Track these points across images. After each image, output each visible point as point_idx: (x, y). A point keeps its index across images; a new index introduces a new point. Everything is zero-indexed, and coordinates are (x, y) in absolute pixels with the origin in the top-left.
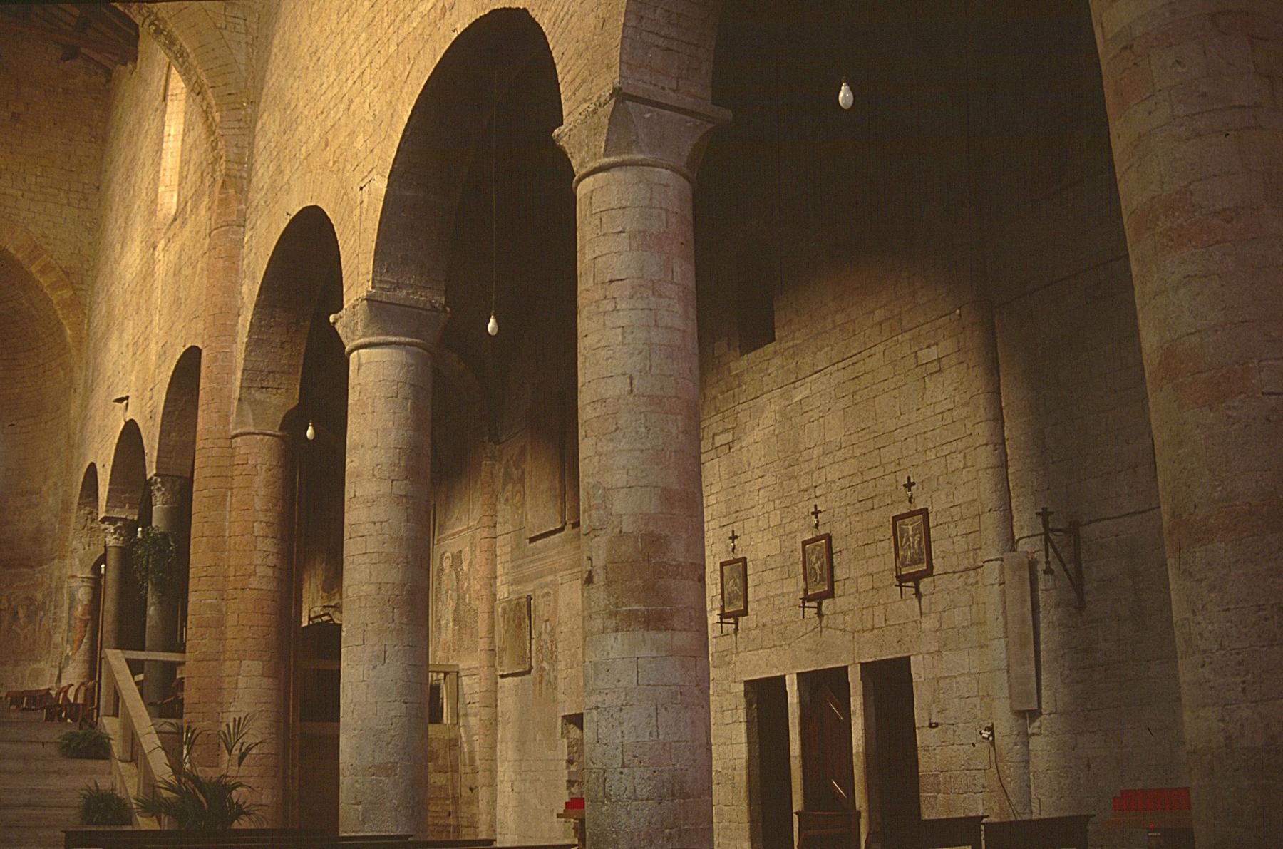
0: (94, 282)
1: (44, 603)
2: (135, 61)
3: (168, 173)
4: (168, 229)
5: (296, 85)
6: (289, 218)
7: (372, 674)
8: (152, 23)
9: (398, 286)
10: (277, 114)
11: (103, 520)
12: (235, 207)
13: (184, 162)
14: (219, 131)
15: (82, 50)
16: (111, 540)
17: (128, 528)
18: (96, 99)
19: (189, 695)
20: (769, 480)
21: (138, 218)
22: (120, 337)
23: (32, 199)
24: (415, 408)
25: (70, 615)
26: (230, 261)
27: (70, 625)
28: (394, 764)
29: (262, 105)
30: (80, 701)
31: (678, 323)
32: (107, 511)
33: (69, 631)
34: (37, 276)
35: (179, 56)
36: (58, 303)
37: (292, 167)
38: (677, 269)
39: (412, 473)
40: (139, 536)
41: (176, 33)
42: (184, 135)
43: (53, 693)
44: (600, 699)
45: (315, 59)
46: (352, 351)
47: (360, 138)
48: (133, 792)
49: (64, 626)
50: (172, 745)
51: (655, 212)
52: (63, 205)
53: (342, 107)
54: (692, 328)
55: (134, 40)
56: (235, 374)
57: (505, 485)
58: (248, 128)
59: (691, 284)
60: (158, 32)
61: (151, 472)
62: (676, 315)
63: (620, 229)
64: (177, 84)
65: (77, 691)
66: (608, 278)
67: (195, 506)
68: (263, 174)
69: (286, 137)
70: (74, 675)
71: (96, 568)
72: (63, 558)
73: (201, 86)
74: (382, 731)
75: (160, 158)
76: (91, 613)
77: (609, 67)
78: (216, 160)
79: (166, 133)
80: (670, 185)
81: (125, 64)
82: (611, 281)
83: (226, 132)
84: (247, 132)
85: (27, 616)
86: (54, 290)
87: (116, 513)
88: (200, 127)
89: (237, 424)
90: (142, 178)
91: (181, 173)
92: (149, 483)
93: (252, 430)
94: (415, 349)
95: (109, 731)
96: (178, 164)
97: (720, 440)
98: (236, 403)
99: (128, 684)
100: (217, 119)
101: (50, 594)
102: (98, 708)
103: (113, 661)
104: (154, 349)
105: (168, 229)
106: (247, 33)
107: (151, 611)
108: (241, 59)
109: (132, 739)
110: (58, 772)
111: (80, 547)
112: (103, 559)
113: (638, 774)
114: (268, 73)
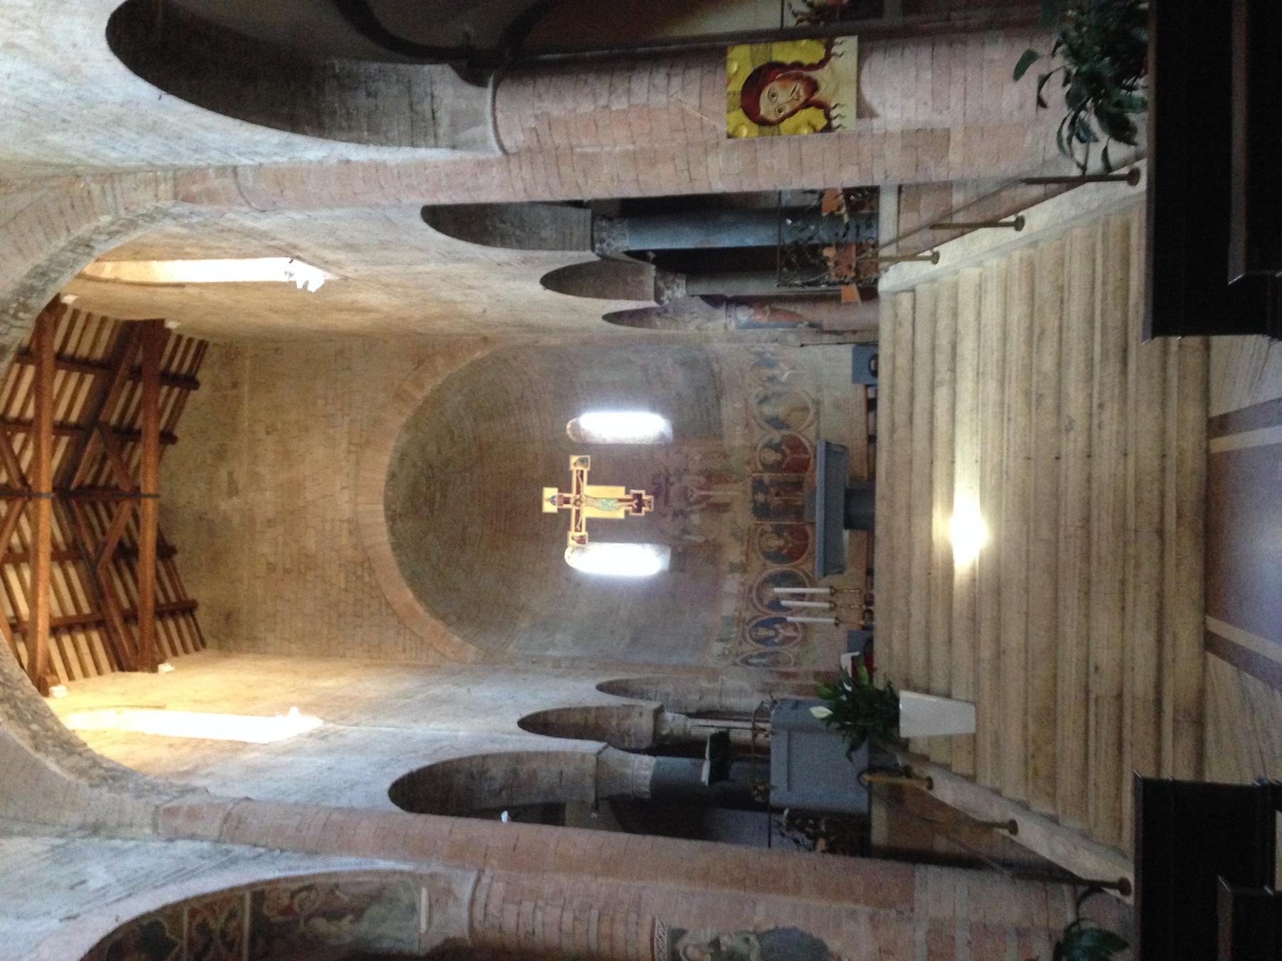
8: (15, 316)
12: (215, 183)
23: (350, 405)
26: (282, 187)
32: (649, 299)
61: (589, 256)
76: (762, 306)
93: (490, 127)
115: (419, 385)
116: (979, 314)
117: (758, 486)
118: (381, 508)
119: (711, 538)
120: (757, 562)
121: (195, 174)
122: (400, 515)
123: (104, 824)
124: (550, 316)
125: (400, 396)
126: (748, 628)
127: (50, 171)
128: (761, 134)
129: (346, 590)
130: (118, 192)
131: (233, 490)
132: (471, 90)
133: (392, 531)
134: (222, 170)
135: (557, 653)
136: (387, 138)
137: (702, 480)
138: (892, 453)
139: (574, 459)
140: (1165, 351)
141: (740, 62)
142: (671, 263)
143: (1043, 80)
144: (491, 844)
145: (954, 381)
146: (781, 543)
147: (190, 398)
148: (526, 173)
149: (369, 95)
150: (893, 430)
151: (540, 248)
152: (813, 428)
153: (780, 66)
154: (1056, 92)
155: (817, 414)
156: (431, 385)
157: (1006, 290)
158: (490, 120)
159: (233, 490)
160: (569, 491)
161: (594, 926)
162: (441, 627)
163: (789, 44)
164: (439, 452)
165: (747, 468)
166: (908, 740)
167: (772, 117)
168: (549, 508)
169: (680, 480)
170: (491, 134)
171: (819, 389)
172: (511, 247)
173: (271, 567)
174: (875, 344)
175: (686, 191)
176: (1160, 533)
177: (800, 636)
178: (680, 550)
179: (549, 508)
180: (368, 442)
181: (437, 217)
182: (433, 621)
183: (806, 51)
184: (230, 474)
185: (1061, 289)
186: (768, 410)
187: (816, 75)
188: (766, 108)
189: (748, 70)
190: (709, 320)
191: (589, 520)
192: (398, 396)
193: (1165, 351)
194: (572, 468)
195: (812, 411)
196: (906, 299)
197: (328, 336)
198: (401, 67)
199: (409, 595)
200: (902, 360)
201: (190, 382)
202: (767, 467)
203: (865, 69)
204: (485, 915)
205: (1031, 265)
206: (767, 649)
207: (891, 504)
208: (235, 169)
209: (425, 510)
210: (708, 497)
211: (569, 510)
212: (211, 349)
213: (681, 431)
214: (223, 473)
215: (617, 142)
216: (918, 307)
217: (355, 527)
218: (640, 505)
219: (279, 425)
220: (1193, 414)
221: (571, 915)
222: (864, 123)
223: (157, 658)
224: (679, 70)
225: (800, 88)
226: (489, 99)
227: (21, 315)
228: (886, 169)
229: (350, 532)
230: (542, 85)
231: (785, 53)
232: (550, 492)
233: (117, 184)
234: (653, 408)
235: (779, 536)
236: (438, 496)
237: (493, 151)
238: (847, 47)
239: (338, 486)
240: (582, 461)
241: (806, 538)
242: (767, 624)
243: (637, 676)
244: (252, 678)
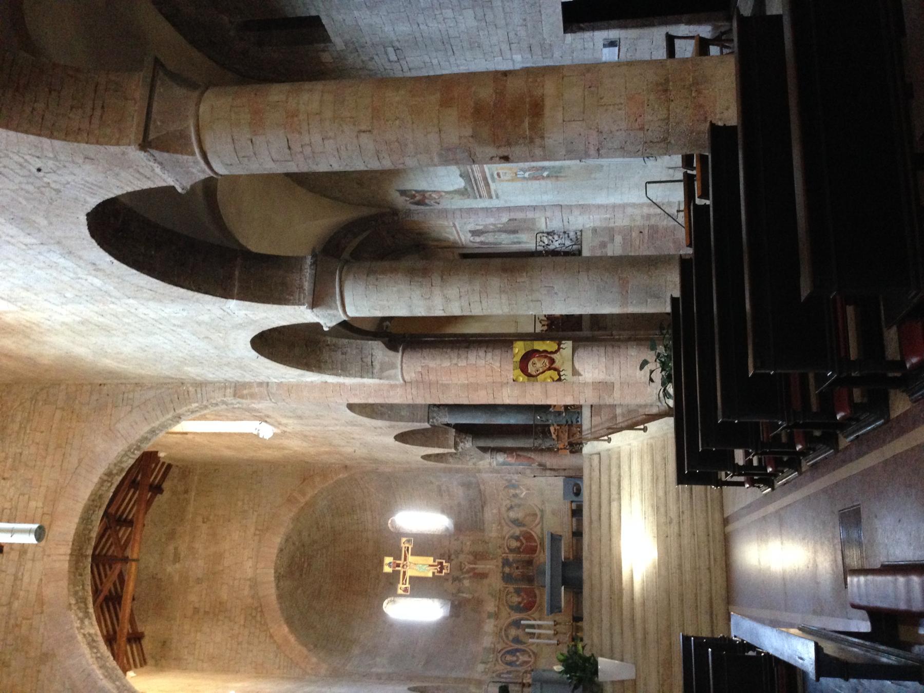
0: (307, 463)
7: (560, 294)
9: (301, 287)
11: (456, 448)
12: (256, 390)
14: (205, 403)
20: (421, 19)
24: (384, 272)
28: (620, 279)
31: (316, 96)
34: (308, 498)
38: (276, 98)
39: (425, 273)
44: (592, 148)
46: (347, 316)
47: (200, 318)
51: (233, 116)
53: (179, 330)
54: (319, 86)
57: (426, 205)
59: (286, 87)
61: (426, 425)
62: (311, 98)
63: (249, 142)
66: (288, 151)
68: (232, 374)
73: (175, 417)
74: (598, 287)
77: (123, 154)
80: (214, 104)
82: (289, 148)
87: (452, 443)
89: (397, 380)
92: (433, 426)
94: (343, 274)
97: (393, 57)
113: (650, 118)
115: (304, 495)
116: (630, 467)
117: (506, 562)
118: (273, 571)
119: (476, 595)
120: (505, 611)
121: (245, 385)
122: (283, 576)
124: (391, 455)
125: (291, 500)
126: (500, 655)
127: (170, 381)
128: (529, 380)
130: (204, 393)
131: (177, 558)
132: (391, 353)
133: (278, 587)
134: (260, 384)
135: (380, 670)
137: (472, 558)
138: (591, 535)
139: (404, 540)
140: (706, 489)
141: (520, 348)
142: (463, 430)
143: (652, 372)
145: (620, 499)
146: (520, 599)
147: (157, 499)
148: (414, 391)
149: (342, 354)
150: (591, 522)
151: (401, 421)
152: (539, 526)
153: (537, 351)
154: (658, 376)
155: (542, 517)
156: (310, 493)
157: (641, 458)
158: (399, 367)
159: (177, 558)
160: (400, 559)
162: (305, 651)
163: (541, 342)
165: (499, 550)
166: (602, 682)
167: (534, 373)
168: (387, 569)
169: (457, 557)
171: (543, 502)
172: (386, 420)
173: (196, 610)
174: (581, 478)
175: (492, 403)
176: (709, 569)
177: (533, 660)
178: (456, 603)
179: (387, 569)
180: (268, 529)
181: (351, 407)
182: (300, 647)
183: (549, 346)
184: (176, 549)
185: (664, 458)
186: (512, 515)
187: (554, 356)
188: (531, 369)
189: (523, 352)
190: (481, 460)
191: (411, 577)
192: (289, 500)
193: (706, 489)
194: (402, 545)
195: (539, 517)
196: (596, 458)
197: (251, 462)
198: (359, 341)
199: (286, 629)
200: (595, 487)
201: (157, 489)
202: (511, 551)
203: (576, 355)
205: (652, 446)
206: (513, 669)
207: (591, 561)
208: (268, 383)
209: (297, 574)
210: (474, 569)
211: (399, 571)
212: (173, 469)
213: (459, 527)
214: (171, 548)
215: (460, 379)
216: (568, 258)
217: (254, 584)
218: (442, 568)
219: (211, 518)
220: (717, 516)
222: (575, 378)
223: (127, 667)
224: (490, 350)
225: (547, 361)
226: (400, 357)
228: (586, 398)
229: (251, 587)
230: (426, 352)
231: (540, 346)
232: (388, 560)
233: (204, 388)
234: (443, 511)
235: (519, 595)
236: (306, 565)
238: (568, 345)
239: (247, 556)
240: (408, 541)
241: (535, 596)
242: (513, 652)
243: (430, 685)
244: (190, 681)
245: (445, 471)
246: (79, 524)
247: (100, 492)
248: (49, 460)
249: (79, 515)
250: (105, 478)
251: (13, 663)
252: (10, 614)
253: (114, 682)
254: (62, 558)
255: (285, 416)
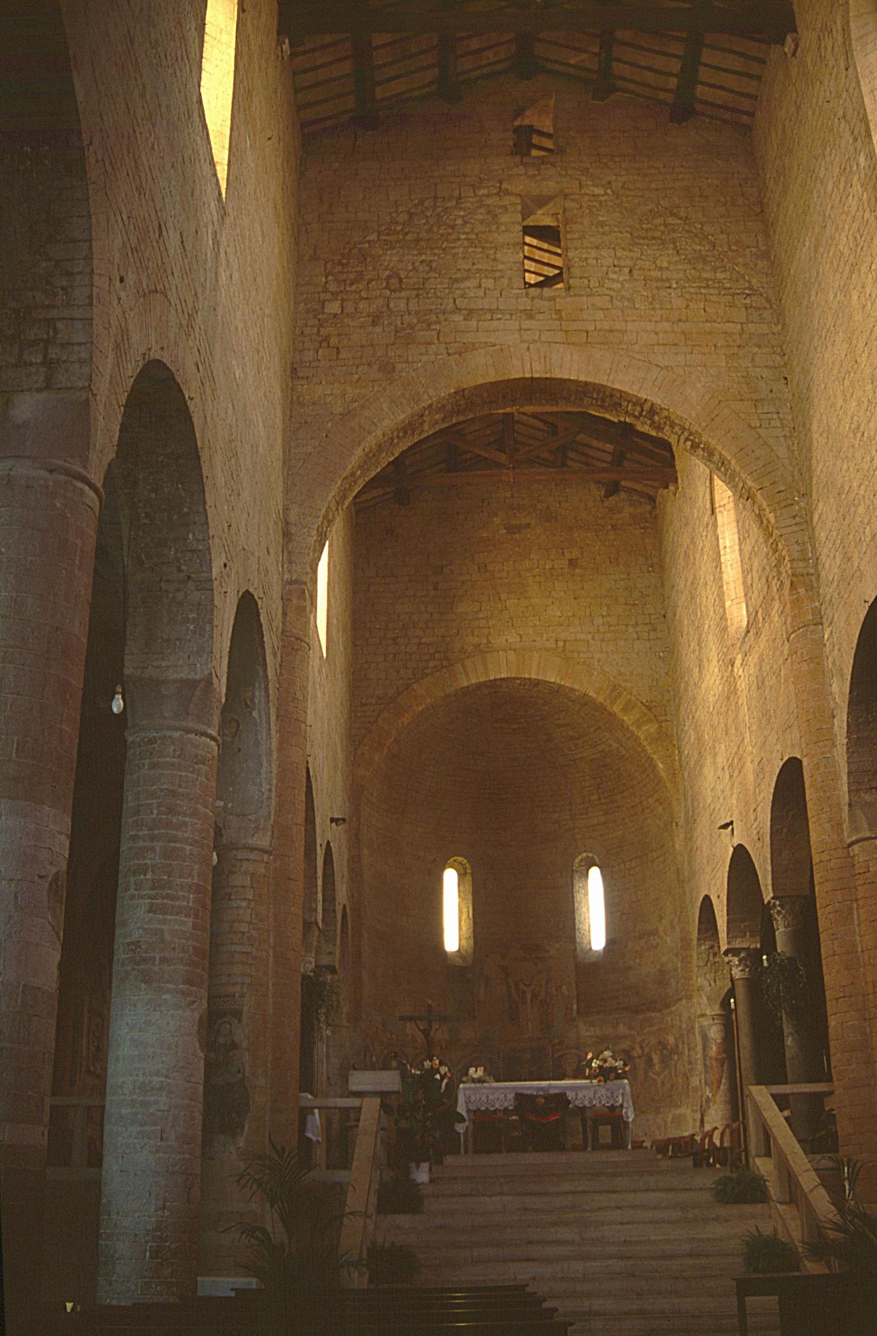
0: (678, 709)
1: (677, 1045)
2: (676, 481)
3: (732, 586)
4: (743, 642)
5: (845, 467)
6: (867, 606)
8: (687, 439)
10: (832, 500)
11: (726, 953)
13: (746, 571)
15: (623, 483)
16: (737, 973)
17: (752, 958)
18: (645, 528)
19: (843, 1127)
21: (710, 636)
22: (714, 763)
23: (602, 640)
25: (705, 1056)
27: (705, 1065)
29: (814, 495)
30: (726, 1145)
32: (729, 943)
33: (706, 1072)
34: (620, 715)
35: (721, 466)
36: (646, 739)
37: (859, 553)
40: (765, 964)
41: (713, 443)
42: (740, 544)
43: (698, 1138)
45: (859, 435)
48: (796, 1235)
49: (700, 1067)
50: (831, 1181)
52: (634, 640)
55: (670, 461)
56: (840, 778)
58: (805, 521)
60: (695, 446)
61: (768, 895)
64: (723, 494)
65: (722, 1134)
67: (822, 923)
68: (830, 565)
69: (846, 522)
70: (716, 1117)
71: (725, 1004)
72: (689, 997)
75: (721, 572)
78: (779, 562)
79: (721, 547)
81: (667, 487)
83: (784, 531)
84: (804, 527)
85: (662, 1061)
86: (639, 727)
87: (737, 944)
88: (755, 530)
89: (849, 836)
90: (707, 596)
91: (745, 583)
92: (768, 907)
93: (868, 834)
95: (763, 1172)
96: (740, 575)
98: (846, 808)
99: (776, 1119)
100: (772, 520)
101: (681, 1036)
102: (746, 1150)
103: (758, 1098)
104: (750, 767)
105: (743, 642)
106: (783, 426)
107: (789, 1041)
108: (782, 452)
109: (789, 1178)
110: (716, 1219)
111: (706, 983)
112: (731, 993)
114: (814, 461)
123: (290, 540)
129: (419, 644)
136: (853, 752)
144: (292, 859)
161: (238, 948)
164: (559, 726)
170: (862, 835)
190: (708, 998)
204: (241, 860)
221: (246, 930)
227: (689, 443)
237: (849, 836)
245: (685, 943)
246: (576, 382)
247: (625, 404)
248: (666, 325)
249: (590, 380)
250: (647, 407)
251: (378, 329)
252: (444, 312)
253: (359, 467)
254: (528, 368)
255: (761, 660)
